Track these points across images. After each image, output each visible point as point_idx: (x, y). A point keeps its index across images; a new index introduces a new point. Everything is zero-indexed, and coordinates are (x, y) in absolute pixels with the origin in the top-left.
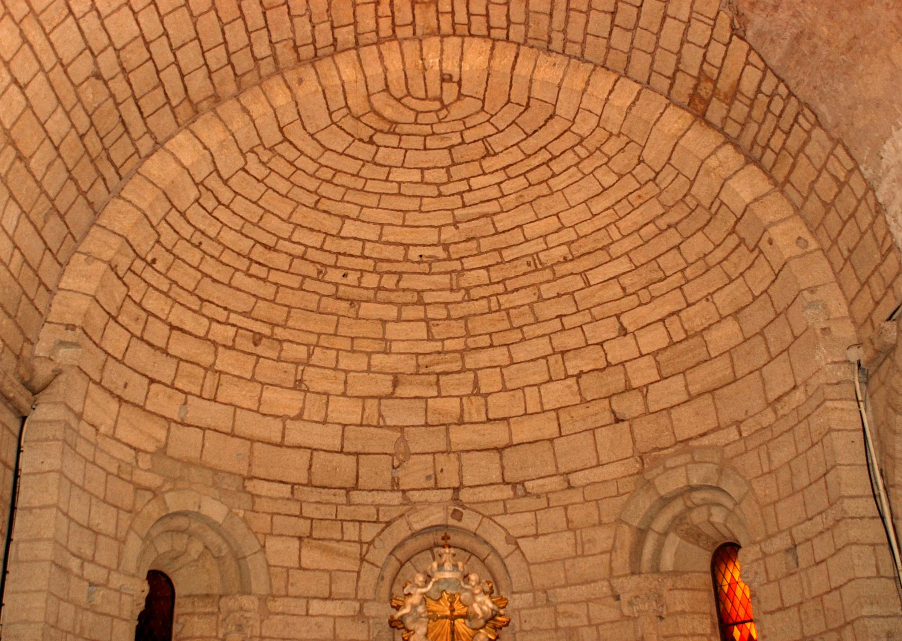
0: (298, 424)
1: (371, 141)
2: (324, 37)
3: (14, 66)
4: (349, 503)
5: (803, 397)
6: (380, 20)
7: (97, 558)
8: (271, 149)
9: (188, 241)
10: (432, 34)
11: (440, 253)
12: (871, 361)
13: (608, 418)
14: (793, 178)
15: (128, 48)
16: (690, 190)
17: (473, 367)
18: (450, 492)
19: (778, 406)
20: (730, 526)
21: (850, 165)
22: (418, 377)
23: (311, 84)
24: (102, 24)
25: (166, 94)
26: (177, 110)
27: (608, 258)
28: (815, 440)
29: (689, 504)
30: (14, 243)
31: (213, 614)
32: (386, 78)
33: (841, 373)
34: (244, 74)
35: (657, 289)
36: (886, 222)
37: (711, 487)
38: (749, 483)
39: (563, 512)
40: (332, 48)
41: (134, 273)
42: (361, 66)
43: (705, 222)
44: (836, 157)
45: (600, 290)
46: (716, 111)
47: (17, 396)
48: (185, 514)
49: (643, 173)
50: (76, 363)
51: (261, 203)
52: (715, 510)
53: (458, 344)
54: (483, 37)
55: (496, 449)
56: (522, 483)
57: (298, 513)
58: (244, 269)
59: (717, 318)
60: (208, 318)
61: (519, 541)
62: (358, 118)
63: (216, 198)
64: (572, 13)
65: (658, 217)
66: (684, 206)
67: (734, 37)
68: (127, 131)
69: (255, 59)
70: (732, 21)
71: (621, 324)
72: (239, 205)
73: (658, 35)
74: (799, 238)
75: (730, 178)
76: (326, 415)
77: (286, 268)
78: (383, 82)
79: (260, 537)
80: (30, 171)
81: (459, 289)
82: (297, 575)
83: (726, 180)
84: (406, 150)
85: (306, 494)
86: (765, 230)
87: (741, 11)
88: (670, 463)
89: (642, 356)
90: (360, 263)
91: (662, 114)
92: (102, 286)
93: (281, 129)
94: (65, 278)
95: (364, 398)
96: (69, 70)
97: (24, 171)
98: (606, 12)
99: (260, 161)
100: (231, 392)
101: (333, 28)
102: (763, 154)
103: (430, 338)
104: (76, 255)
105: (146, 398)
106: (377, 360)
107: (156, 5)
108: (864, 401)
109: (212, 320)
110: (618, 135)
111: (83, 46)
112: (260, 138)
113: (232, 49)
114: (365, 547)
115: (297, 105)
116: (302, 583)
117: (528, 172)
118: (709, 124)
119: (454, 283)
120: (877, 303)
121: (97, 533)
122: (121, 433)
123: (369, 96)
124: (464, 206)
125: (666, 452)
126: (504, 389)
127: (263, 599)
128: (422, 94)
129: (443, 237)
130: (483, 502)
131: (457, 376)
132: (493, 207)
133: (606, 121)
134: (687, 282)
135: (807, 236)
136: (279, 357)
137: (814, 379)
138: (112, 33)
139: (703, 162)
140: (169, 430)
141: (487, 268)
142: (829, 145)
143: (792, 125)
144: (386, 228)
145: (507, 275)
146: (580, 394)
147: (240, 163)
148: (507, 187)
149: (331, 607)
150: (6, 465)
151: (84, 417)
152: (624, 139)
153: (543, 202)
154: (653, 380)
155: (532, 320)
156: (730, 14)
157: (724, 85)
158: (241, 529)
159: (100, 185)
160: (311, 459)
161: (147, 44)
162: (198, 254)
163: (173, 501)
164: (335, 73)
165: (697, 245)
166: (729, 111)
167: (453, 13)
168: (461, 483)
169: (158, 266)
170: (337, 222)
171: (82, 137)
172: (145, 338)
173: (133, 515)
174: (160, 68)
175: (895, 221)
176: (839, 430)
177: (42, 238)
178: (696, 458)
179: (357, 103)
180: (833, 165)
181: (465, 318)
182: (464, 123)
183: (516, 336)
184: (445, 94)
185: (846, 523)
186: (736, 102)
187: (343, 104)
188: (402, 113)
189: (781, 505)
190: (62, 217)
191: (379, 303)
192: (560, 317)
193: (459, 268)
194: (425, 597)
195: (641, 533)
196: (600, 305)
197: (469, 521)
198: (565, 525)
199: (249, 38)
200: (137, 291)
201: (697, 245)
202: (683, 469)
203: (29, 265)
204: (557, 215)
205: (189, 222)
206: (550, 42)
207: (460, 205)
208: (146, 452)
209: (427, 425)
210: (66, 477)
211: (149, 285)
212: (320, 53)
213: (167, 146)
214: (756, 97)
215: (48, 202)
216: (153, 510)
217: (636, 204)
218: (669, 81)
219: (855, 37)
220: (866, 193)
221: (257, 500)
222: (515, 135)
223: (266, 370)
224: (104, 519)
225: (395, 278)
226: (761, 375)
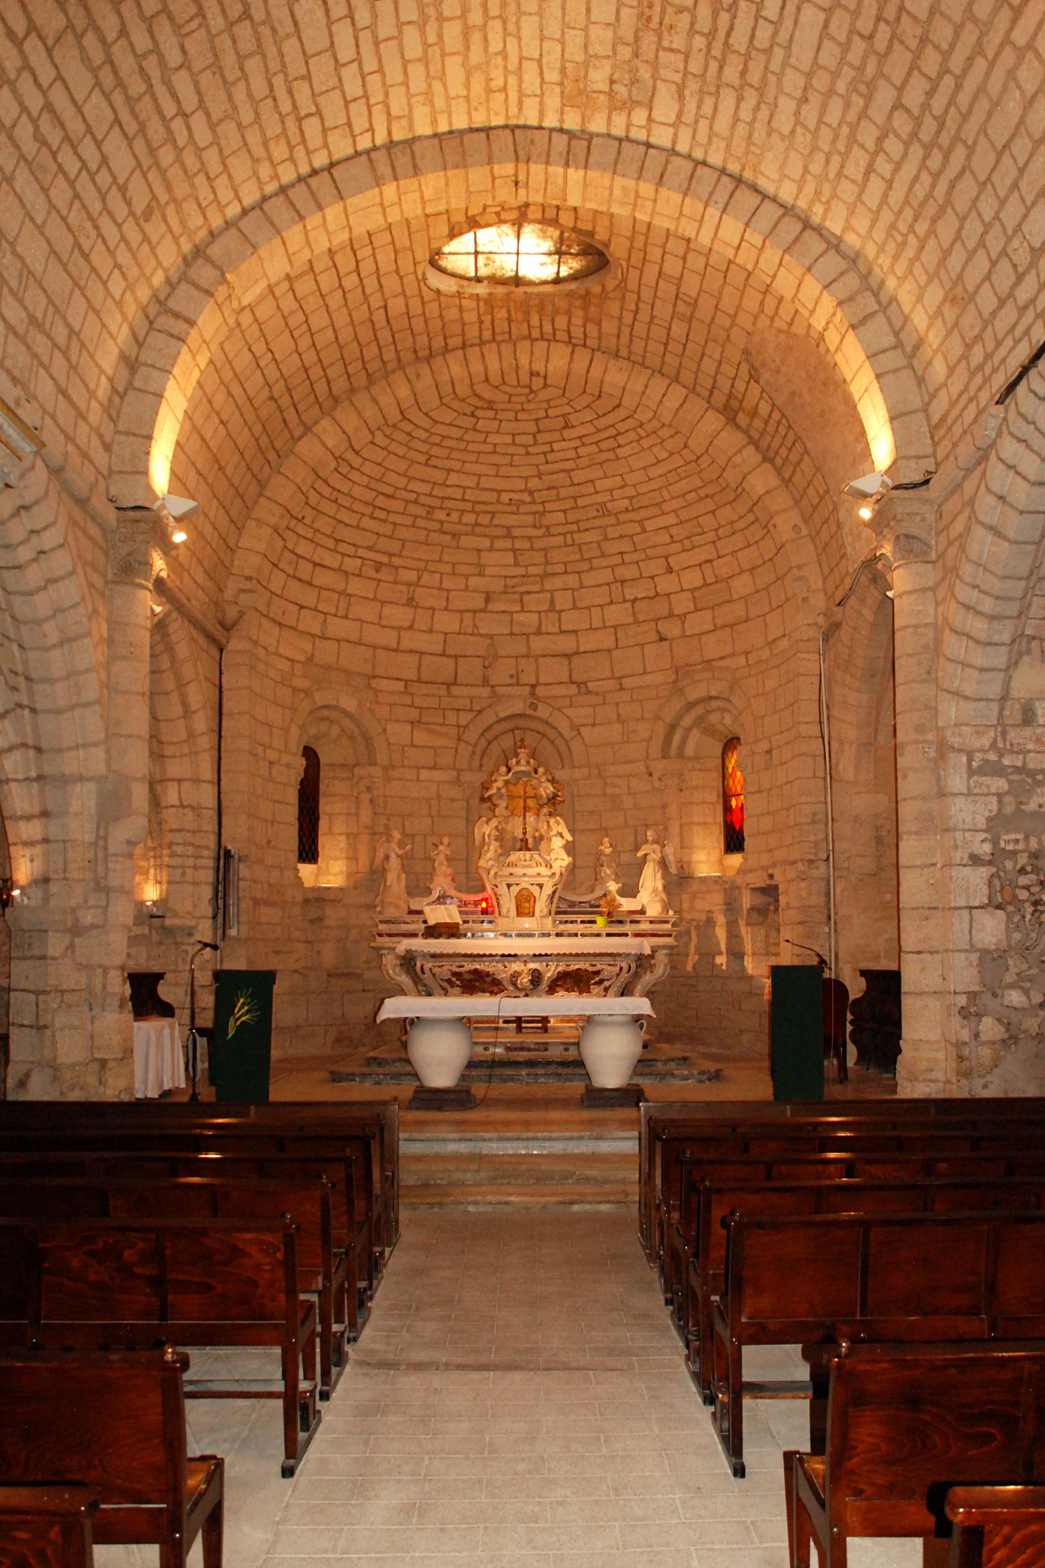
0: (409, 633)
1: (473, 415)
2: (438, 343)
4: (450, 695)
10: (525, 338)
13: (654, 637)
33: (812, 633)
46: (742, 419)
48: (327, 707)
52: (726, 715)
85: (414, 688)
88: (697, 677)
90: (461, 505)
100: (359, 610)
103: (516, 564)
106: (474, 581)
109: (343, 555)
118: (738, 427)
126: (575, 608)
127: (385, 769)
132: (570, 465)
135: (801, 524)
141: (564, 511)
148: (582, 451)
149: (436, 775)
159: (267, 468)
162: (335, 506)
163: (320, 698)
169: (307, 521)
170: (444, 474)
179: (463, 390)
181: (545, 550)
183: (585, 566)
194: (507, 782)
195: (672, 728)
197: (543, 711)
201: (727, 514)
209: (512, 634)
216: (306, 706)
222: (588, 415)
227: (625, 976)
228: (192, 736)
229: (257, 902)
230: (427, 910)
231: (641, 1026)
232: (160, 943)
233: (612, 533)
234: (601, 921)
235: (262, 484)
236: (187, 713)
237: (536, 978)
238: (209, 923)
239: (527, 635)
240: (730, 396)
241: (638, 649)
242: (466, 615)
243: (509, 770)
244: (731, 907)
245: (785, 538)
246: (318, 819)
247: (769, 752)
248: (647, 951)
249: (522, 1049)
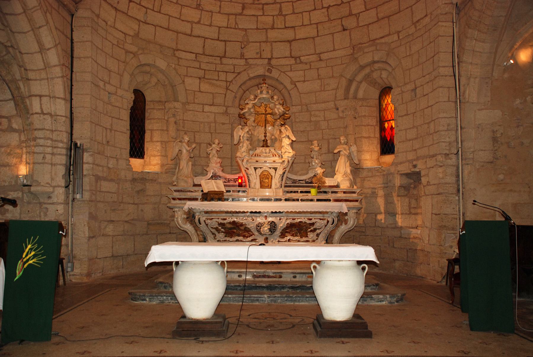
4: (221, 64)
13: (340, 28)
20: (389, 79)
22: (254, 5)
28: (431, 40)
29: (373, 69)
31: (162, 109)
48: (148, 65)
52: (383, 72)
55: (288, 41)
56: (299, 57)
61: (296, 83)
79: (182, 76)
108: (456, 23)
114: (228, 83)
121: (110, 71)
122: (118, 26)
126: (294, 13)
127: (184, 104)
131: (272, 6)
140: (139, 25)
146: (328, 17)
149: (213, 109)
163: (144, 59)
194: (254, 105)
195: (350, 82)
197: (275, 74)
202: (372, 53)
209: (257, 29)
224: (112, 65)
226: (412, 9)
227: (330, 227)
228: (47, 66)
229: (98, 178)
230: (203, 183)
231: (363, 269)
232: (29, 203)
234: (313, 191)
236: (42, 49)
237: (273, 227)
238: (62, 190)
239: (266, 29)
241: (331, 36)
242: (231, 17)
243: (256, 97)
244: (387, 186)
246: (144, 132)
248: (345, 210)
249: (264, 276)
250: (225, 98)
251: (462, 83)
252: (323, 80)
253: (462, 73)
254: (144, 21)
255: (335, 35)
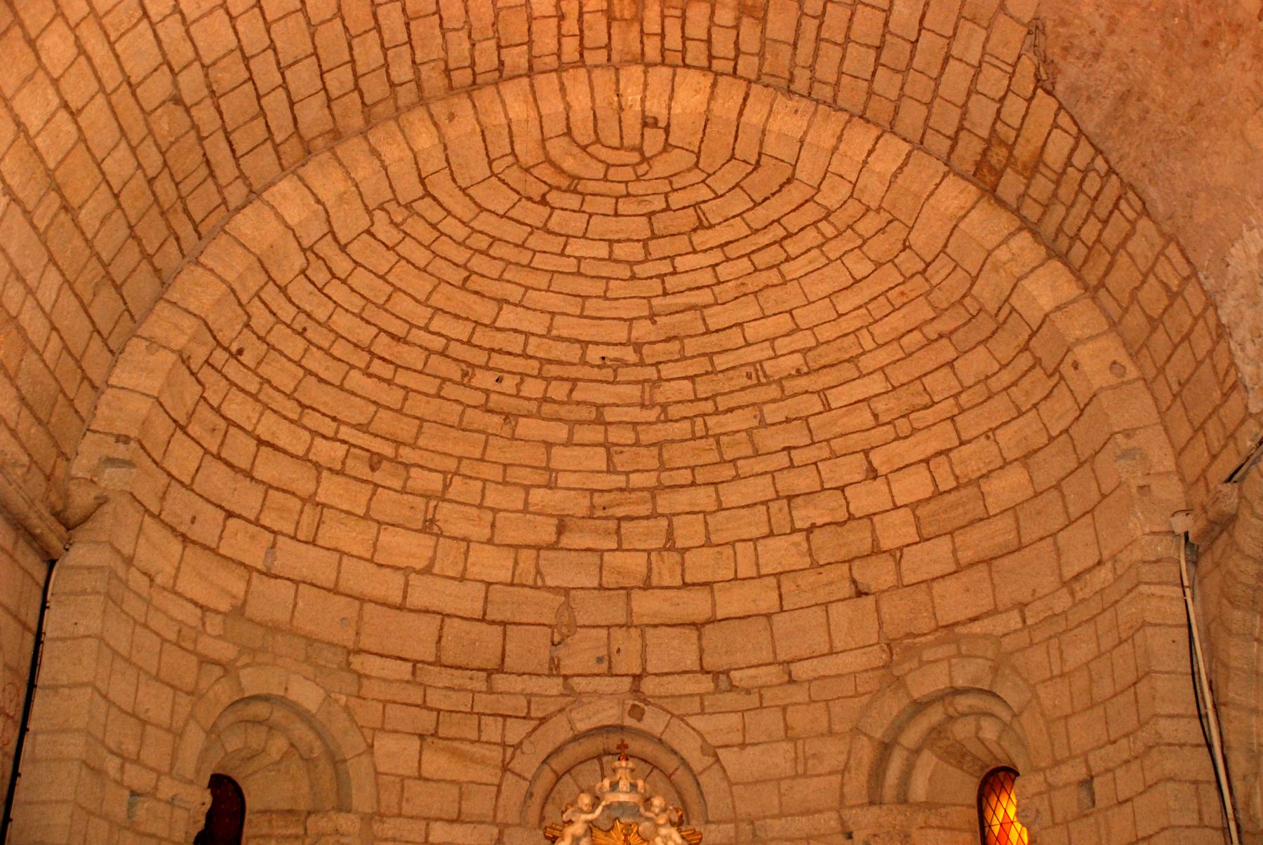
0: (427, 579)
1: (543, 201)
3: (64, 85)
4: (490, 691)
5: (1110, 576)
6: (564, 40)
7: (143, 756)
8: (408, 206)
9: (288, 326)
10: (634, 62)
11: (630, 355)
12: (1204, 533)
14: (1110, 282)
15: (221, 64)
16: (970, 288)
17: (667, 511)
18: (629, 680)
19: (1077, 586)
20: (1005, 744)
21: (1186, 271)
22: (591, 522)
23: (466, 122)
24: (187, 32)
25: (268, 126)
26: (281, 148)
27: (857, 375)
28: (1124, 636)
29: (951, 711)
30: (51, 322)
31: (297, 837)
32: (568, 118)
33: (1163, 547)
34: (375, 104)
35: (920, 418)
36: (1230, 350)
37: (981, 691)
38: (1032, 688)
39: (780, 716)
40: (497, 74)
41: (213, 367)
42: (535, 100)
43: (989, 334)
44: (1167, 258)
45: (844, 415)
46: (1010, 185)
47: (46, 531)
48: (265, 698)
49: (909, 263)
50: (128, 488)
51: (390, 278)
52: (986, 723)
53: (648, 480)
54: (701, 68)
55: (693, 624)
56: (726, 673)
57: (420, 702)
58: (363, 365)
59: (999, 462)
60: (310, 431)
61: (720, 751)
62: (527, 170)
63: (329, 269)
64: (823, 45)
65: (926, 322)
66: (962, 311)
67: (1039, 91)
68: (212, 174)
69: (392, 85)
70: (1038, 69)
71: (870, 463)
72: (360, 280)
73: (937, 81)
74: (1114, 363)
75: (1026, 276)
76: (465, 569)
77: (420, 367)
78: (564, 123)
79: (368, 733)
80: (77, 226)
81: (653, 406)
82: (414, 787)
83: (1019, 279)
84: (591, 215)
86: (1069, 350)
87: (1050, 57)
88: (928, 655)
89: (896, 507)
90: (520, 364)
91: (938, 185)
92: (169, 383)
93: (422, 181)
94: (117, 371)
95: (517, 547)
96: (139, 91)
97: (69, 225)
98: (869, 47)
99: (392, 222)
100: (337, 533)
101: (499, 47)
102: (1070, 247)
104: (135, 340)
105: (221, 538)
106: (537, 496)
107: (261, 8)
108: (1192, 587)
109: (314, 433)
110: (878, 210)
111: (160, 59)
112: (394, 191)
113: (361, 70)
114: (509, 751)
115: (445, 148)
116: (422, 799)
117: (753, 252)
118: (1001, 203)
119: (647, 396)
120: (1214, 457)
121: (144, 723)
122: (184, 586)
123: (543, 140)
124: (665, 294)
125: (923, 639)
126: (708, 544)
127: (367, 819)
128: (615, 142)
129: (634, 334)
130: (673, 696)
131: (645, 523)
132: (705, 297)
133: (862, 191)
134: (962, 411)
135: (1123, 359)
136: (404, 487)
137: (1125, 553)
138: (200, 45)
139: (989, 253)
140: (249, 582)
141: (692, 378)
142: (1159, 241)
143: (1111, 212)
144: (558, 318)
145: (719, 388)
146: (811, 555)
147: (365, 223)
148: (724, 271)
150: (24, 626)
151: (135, 563)
152: (885, 216)
153: (770, 293)
154: (910, 540)
155: (750, 452)
156: (1035, 60)
157: (1023, 152)
158: (341, 721)
159: (172, 247)
160: (442, 628)
161: (246, 59)
162: (301, 344)
163: (252, 681)
164: (499, 108)
165: (976, 364)
166: (1028, 187)
167: (663, 35)
168: (644, 669)
169: (246, 358)
170: (493, 306)
171: (151, 181)
172: (223, 455)
173: (194, 698)
174: (261, 93)
175: (1243, 350)
176: (1156, 625)
177: (90, 317)
178: (964, 649)
179: (527, 150)
180: (1163, 269)
181: (659, 445)
182: (671, 183)
183: (727, 472)
184: (646, 142)
185: (1160, 752)
186: (1038, 176)
187: (508, 150)
188: (587, 166)
189: (1073, 722)
190: (118, 288)
191: (543, 419)
192: (788, 449)
193: (655, 376)
194: (591, 827)
195: (885, 749)
196: (842, 435)
197: (653, 722)
198: (782, 733)
199: (385, 56)
200: (215, 392)
201: (976, 364)
202: (945, 664)
203: (70, 353)
204: (790, 312)
205: (290, 301)
206: (791, 80)
207: (660, 292)
208: (217, 612)
209: (601, 588)
210: (108, 645)
211: (232, 384)
212: (479, 80)
213: (265, 195)
214: (1064, 172)
215: (100, 267)
216: (224, 693)
217: (897, 304)
218: (949, 142)
219: (1200, 104)
220: (1205, 309)
221: (365, 682)
223: (387, 505)
224: (156, 703)
225: (567, 386)
226: (1055, 544)
233: (773, 413)
235: (164, 281)
240: (994, 139)
241: (819, 612)
243: (597, 800)
245: (1097, 382)
247: (1087, 783)
250: (497, 797)
251: (1236, 771)
252: (800, 743)
253: (1231, 738)
254: (264, 570)
255: (833, 609)
